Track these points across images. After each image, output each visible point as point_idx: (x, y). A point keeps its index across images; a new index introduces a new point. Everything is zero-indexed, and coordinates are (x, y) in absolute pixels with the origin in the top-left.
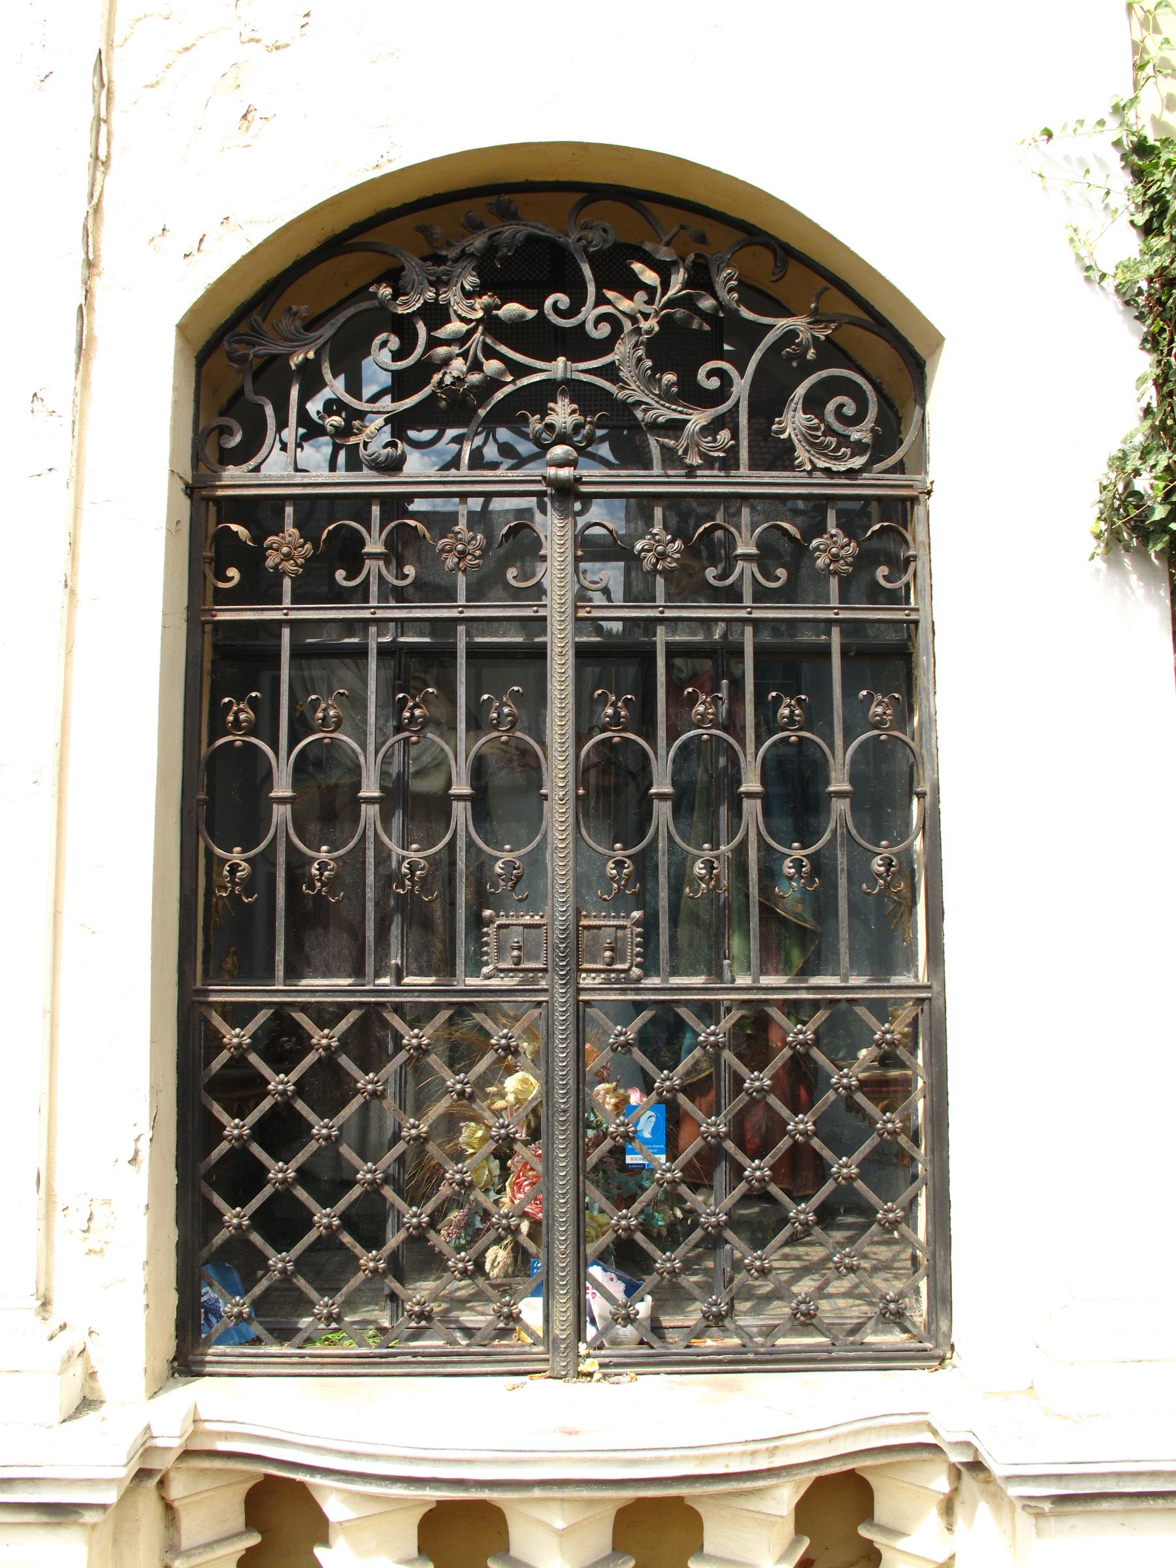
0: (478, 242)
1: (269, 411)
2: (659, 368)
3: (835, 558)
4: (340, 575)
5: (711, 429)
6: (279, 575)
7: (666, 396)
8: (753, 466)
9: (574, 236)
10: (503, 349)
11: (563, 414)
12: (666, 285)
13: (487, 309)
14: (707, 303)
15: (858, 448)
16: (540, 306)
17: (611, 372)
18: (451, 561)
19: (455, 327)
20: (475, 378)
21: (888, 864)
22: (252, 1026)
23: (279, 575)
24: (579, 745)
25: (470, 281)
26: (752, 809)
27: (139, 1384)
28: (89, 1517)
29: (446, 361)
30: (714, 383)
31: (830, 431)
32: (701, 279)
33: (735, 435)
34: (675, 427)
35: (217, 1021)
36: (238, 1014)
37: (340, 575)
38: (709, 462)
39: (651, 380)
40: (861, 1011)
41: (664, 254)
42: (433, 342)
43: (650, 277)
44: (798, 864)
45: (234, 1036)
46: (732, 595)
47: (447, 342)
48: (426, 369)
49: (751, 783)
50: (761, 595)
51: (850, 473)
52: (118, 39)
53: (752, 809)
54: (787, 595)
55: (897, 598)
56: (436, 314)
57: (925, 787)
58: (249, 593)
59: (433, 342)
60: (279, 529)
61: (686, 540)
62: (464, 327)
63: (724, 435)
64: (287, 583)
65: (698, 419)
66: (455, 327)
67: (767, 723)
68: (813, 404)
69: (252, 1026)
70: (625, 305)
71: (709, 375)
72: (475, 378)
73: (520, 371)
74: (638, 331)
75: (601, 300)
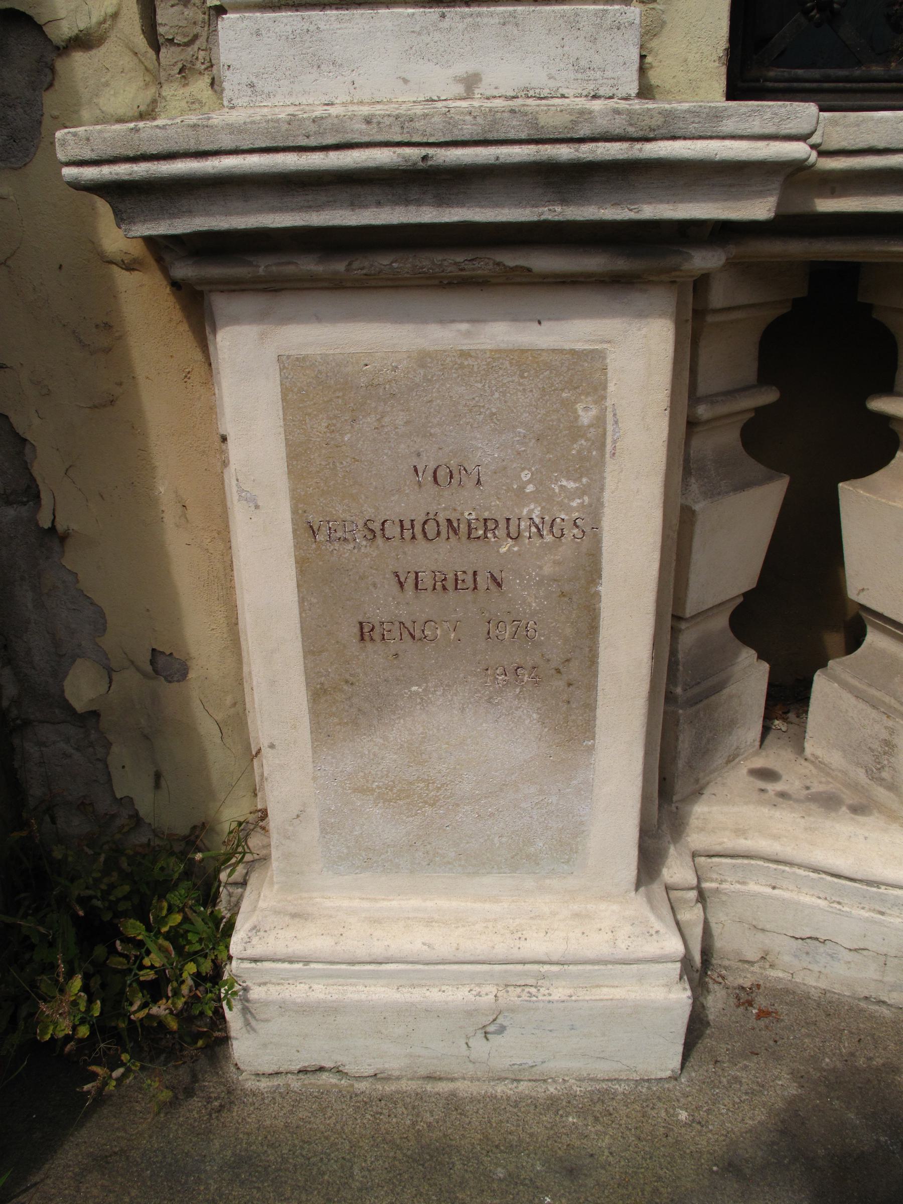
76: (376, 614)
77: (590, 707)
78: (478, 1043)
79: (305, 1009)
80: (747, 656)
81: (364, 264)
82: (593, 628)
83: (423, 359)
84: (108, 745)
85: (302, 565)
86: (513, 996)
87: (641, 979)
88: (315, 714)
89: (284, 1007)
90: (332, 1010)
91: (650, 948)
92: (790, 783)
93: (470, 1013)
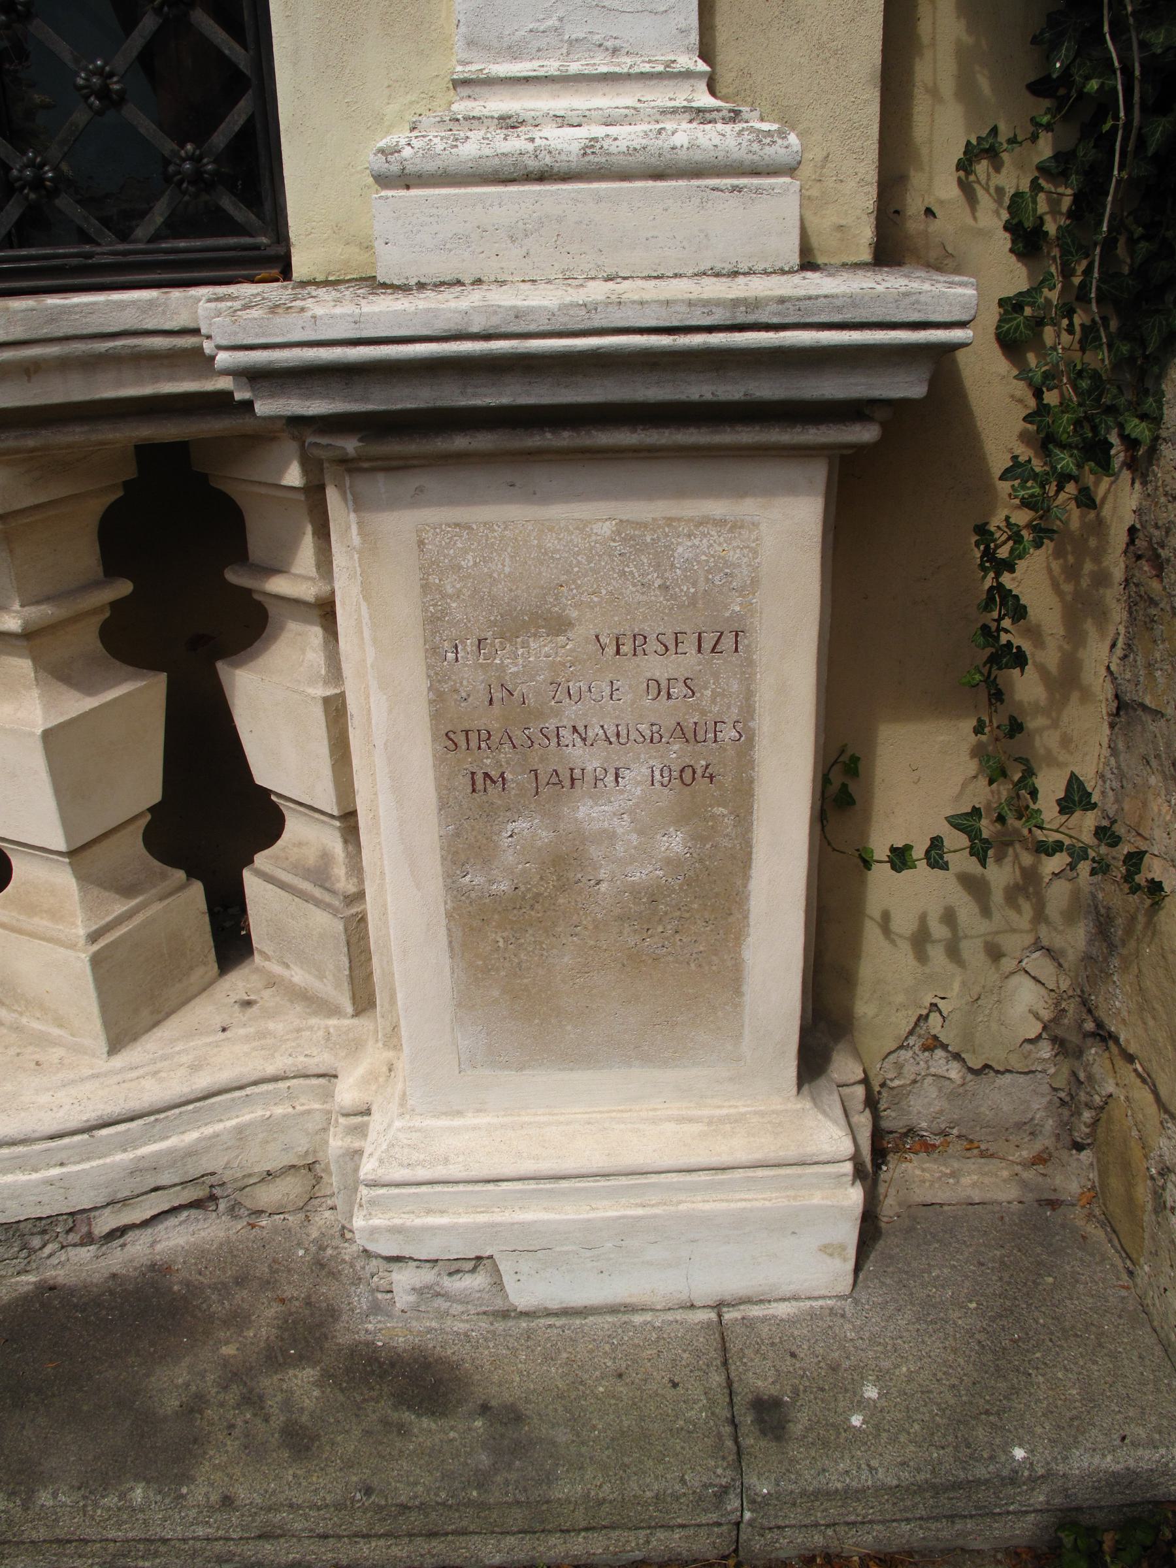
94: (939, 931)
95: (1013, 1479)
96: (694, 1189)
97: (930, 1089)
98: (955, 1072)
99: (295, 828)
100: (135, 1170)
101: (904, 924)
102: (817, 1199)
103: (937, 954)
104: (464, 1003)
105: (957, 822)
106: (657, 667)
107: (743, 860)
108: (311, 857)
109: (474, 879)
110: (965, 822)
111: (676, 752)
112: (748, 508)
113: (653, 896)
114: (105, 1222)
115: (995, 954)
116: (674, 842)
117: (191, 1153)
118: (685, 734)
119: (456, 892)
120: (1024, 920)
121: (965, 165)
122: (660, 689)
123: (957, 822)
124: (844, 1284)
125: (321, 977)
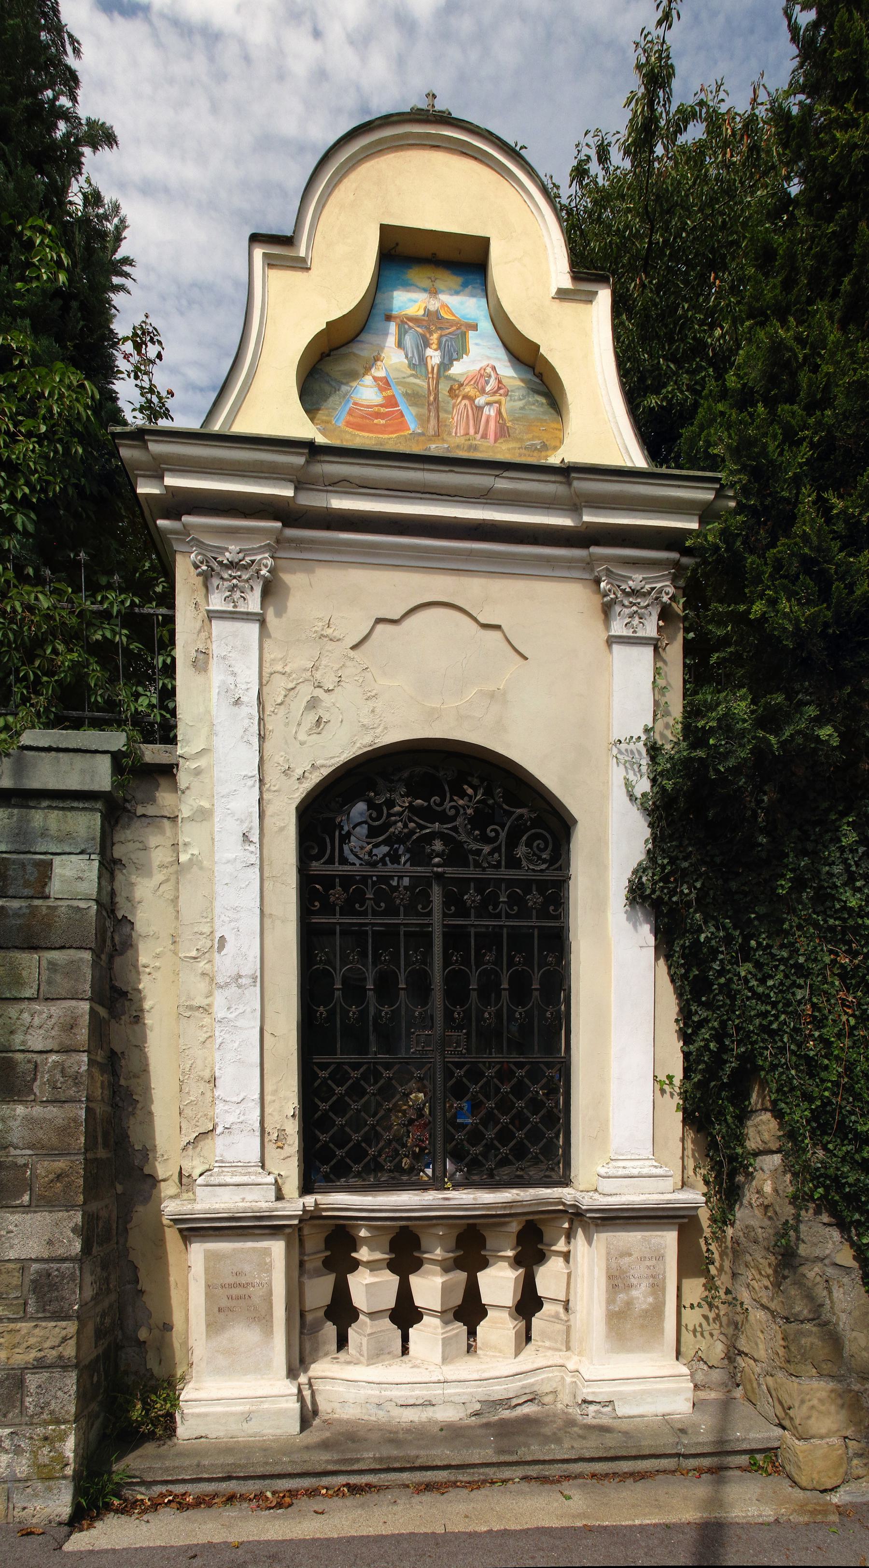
0: (406, 774)
1: (328, 840)
2: (474, 829)
3: (535, 903)
4: (357, 905)
5: (491, 853)
6: (335, 905)
7: (476, 839)
8: (506, 867)
9: (442, 773)
10: (416, 819)
11: (438, 845)
12: (476, 795)
13: (410, 803)
14: (491, 802)
15: (544, 861)
16: (428, 801)
17: (455, 829)
18: (398, 901)
19: (397, 809)
20: (406, 830)
21: (552, 1014)
22: (329, 1070)
23: (335, 905)
24: (444, 970)
25: (403, 790)
26: (505, 994)
27: (296, 1194)
28: (288, 1231)
29: (395, 822)
30: (493, 834)
31: (534, 854)
32: (488, 792)
33: (500, 856)
34: (478, 852)
35: (316, 1069)
36: (323, 1066)
37: (357, 905)
38: (491, 866)
39: (469, 833)
40: (542, 1066)
41: (476, 782)
42: (390, 815)
43: (470, 791)
44: (520, 1014)
45: (323, 1074)
46: (498, 916)
47: (394, 815)
48: (387, 825)
49: (505, 985)
50: (508, 916)
51: (542, 871)
52: (264, 682)
53: (505, 994)
54: (517, 916)
55: (557, 917)
56: (390, 804)
57: (566, 987)
58: (322, 912)
59: (390, 815)
60: (334, 888)
61: (482, 895)
62: (401, 809)
63: (496, 855)
64: (338, 908)
65: (487, 849)
66: (397, 809)
67: (511, 963)
68: (529, 844)
69: (329, 1070)
70: (461, 802)
71: (492, 831)
72: (406, 830)
73: (422, 827)
74: (465, 813)
75: (452, 800)
76: (222, 1305)
77: (272, 1327)
78: (244, 1424)
79: (199, 1415)
80: (329, 1323)
81: (222, 1232)
82: (271, 1307)
83: (234, 1249)
84: (146, 1352)
85: (206, 1294)
86: (254, 1408)
87: (287, 1401)
88: (207, 1331)
89: (193, 1415)
90: (206, 1415)
91: (289, 1392)
92: (342, 1359)
93: (242, 1414)
94: (699, 1329)
95: (738, 1440)
96: (656, 1382)
97: (700, 1372)
98: (705, 1367)
99: (547, 1307)
100: (523, 1387)
101: (691, 1327)
102: (683, 1385)
103: (698, 1334)
104: (607, 1336)
105: (703, 1299)
106: (648, 1263)
107: (664, 1303)
108: (553, 1313)
109: (611, 1307)
110: (705, 1299)
111: (651, 1280)
112: (665, 1233)
113: (646, 1311)
114: (514, 1402)
115: (712, 1335)
116: (650, 1300)
117: (533, 1385)
118: (653, 1277)
119: (608, 1310)
120: (717, 1327)
121: (695, 1170)
122: (648, 1267)
123: (703, 1299)
124: (691, 1410)
125: (556, 1342)
